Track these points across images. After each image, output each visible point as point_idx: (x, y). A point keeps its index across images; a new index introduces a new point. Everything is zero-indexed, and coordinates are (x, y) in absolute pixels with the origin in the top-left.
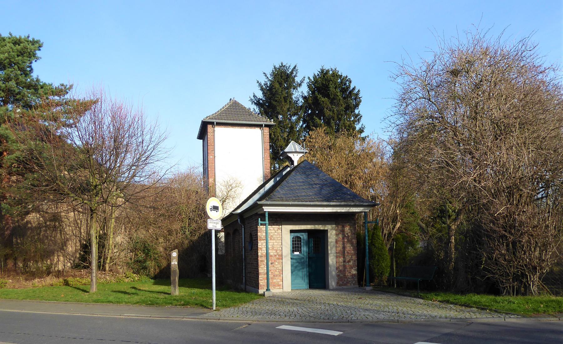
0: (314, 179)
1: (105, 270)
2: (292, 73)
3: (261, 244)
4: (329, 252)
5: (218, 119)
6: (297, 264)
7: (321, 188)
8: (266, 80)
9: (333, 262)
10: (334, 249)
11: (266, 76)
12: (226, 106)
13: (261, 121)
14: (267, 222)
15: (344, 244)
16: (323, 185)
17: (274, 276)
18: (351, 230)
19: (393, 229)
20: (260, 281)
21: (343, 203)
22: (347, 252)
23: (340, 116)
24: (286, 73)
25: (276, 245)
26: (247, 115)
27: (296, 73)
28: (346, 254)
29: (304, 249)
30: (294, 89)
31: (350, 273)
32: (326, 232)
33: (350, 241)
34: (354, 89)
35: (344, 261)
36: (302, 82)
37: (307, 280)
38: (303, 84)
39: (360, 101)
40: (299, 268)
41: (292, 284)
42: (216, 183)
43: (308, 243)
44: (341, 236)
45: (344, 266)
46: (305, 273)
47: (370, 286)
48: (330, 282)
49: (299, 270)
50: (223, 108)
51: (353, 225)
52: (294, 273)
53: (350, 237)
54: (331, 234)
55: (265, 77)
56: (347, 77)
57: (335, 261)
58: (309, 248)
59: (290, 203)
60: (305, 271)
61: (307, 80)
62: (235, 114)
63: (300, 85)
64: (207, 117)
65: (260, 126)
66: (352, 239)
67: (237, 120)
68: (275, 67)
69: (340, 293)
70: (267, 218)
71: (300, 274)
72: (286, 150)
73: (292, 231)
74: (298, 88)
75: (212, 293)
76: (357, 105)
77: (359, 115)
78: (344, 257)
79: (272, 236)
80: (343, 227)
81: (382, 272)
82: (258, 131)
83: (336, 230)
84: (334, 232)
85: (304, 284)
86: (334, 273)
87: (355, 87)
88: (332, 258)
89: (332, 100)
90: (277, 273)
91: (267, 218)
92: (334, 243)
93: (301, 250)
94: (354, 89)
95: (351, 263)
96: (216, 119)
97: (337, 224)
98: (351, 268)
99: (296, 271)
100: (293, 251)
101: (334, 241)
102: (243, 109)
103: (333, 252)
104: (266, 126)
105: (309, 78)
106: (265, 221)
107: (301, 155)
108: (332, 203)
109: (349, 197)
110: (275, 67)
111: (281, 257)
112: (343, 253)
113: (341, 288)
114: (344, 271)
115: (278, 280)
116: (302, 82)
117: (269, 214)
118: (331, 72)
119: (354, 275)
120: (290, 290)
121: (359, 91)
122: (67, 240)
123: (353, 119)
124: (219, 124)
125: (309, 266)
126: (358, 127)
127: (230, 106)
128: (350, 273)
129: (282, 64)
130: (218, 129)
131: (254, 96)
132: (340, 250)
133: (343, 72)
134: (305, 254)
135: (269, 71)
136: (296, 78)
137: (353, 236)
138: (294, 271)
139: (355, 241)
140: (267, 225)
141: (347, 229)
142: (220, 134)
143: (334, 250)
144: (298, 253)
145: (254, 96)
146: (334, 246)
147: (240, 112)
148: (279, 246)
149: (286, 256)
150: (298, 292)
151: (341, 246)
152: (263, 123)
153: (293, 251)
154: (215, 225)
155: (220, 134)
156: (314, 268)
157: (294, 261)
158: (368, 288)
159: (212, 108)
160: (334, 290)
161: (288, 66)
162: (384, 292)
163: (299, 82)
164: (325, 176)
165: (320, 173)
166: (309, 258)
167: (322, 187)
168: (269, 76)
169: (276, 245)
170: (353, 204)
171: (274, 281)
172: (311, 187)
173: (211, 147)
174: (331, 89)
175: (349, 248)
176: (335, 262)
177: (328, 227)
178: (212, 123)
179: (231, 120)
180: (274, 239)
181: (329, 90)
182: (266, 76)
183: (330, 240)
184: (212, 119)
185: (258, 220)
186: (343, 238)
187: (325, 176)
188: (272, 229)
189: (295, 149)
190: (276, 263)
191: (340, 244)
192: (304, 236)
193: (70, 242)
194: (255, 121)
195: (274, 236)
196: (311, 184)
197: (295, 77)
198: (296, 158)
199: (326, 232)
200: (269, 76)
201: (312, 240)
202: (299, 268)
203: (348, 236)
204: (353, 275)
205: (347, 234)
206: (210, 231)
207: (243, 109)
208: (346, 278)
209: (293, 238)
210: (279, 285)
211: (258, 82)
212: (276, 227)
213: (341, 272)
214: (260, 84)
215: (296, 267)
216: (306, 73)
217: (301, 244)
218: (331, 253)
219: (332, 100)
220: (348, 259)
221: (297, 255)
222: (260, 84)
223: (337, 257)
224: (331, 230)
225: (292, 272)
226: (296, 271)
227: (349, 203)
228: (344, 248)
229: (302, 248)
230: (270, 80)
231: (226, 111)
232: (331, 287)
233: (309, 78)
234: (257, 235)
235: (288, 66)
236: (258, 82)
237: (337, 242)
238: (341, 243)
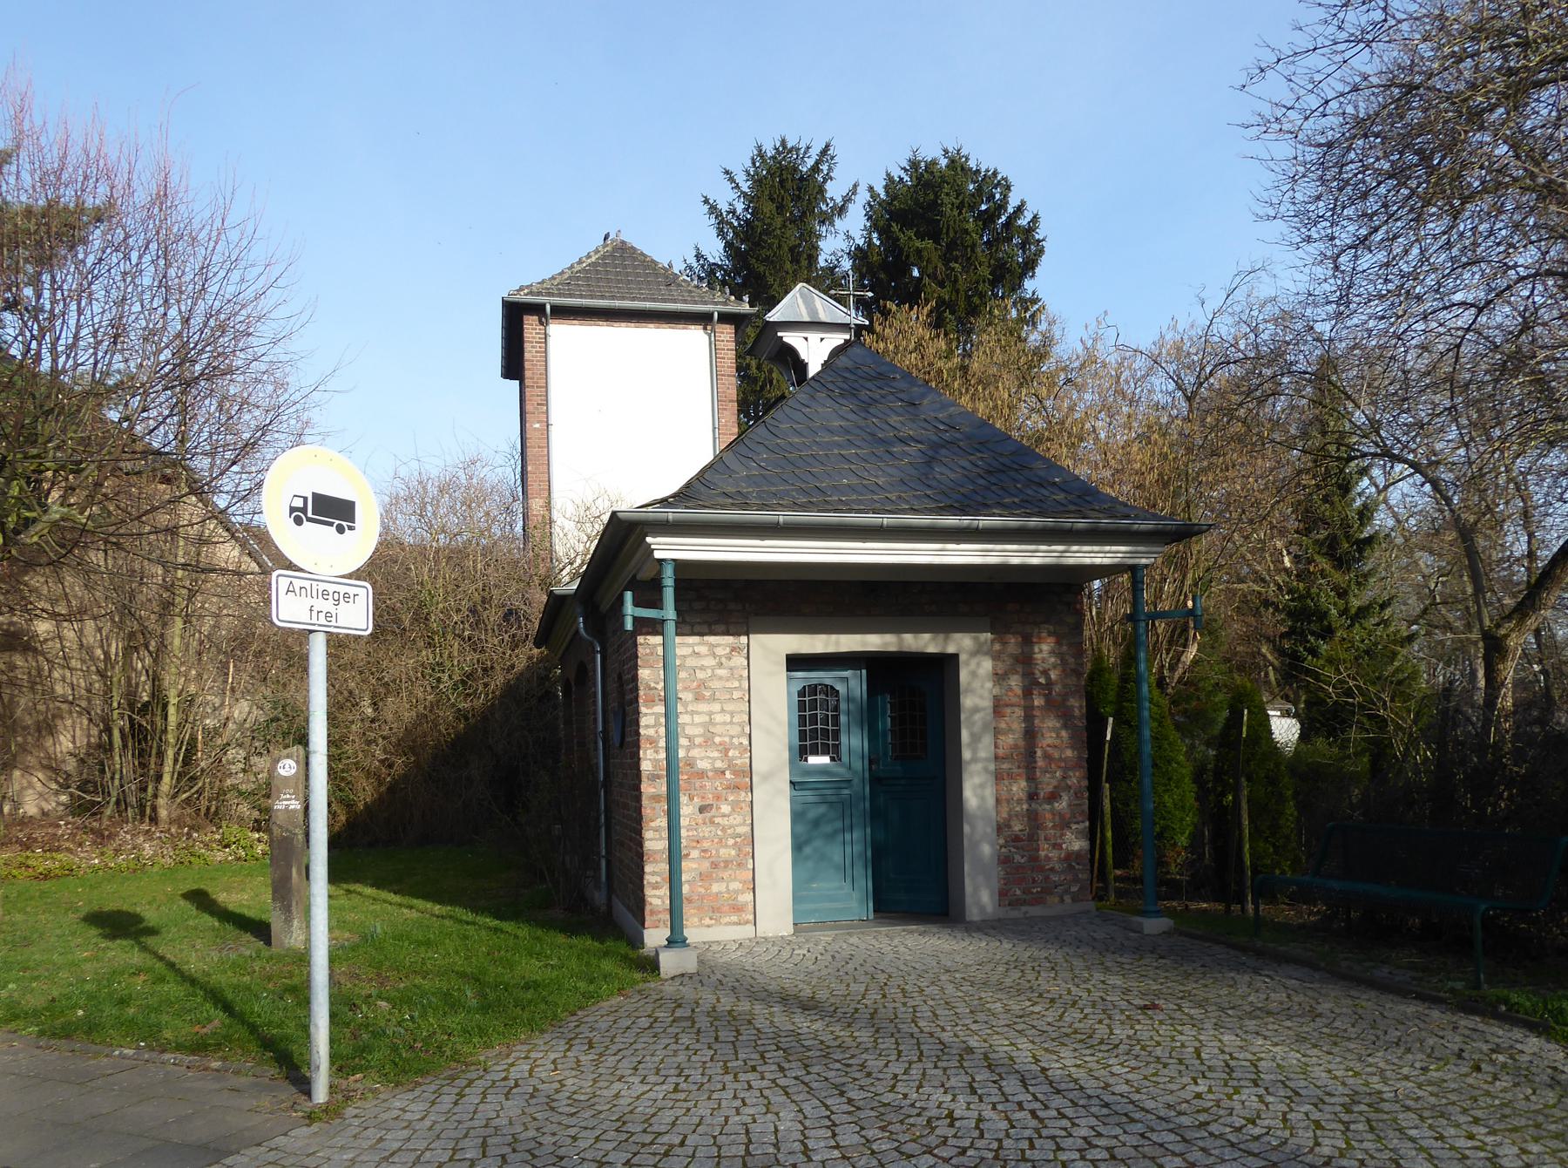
0: (894, 420)
1: (154, 820)
2: (815, 169)
3: (650, 720)
4: (966, 755)
5: (560, 295)
6: (822, 809)
7: (930, 461)
8: (733, 195)
9: (983, 799)
10: (987, 740)
11: (732, 180)
12: (589, 256)
13: (705, 303)
14: (669, 612)
15: (1028, 717)
16: (935, 447)
17: (715, 865)
18: (1061, 656)
19: (1172, 668)
20: (648, 892)
21: (1034, 522)
22: (1047, 756)
23: (976, 300)
24: (796, 169)
25: (725, 728)
26: (659, 283)
27: (830, 169)
28: (1040, 763)
29: (854, 741)
30: (822, 222)
31: (1057, 846)
32: (946, 664)
33: (1056, 706)
34: (1020, 210)
35: (1032, 796)
36: (847, 199)
37: (865, 883)
38: (851, 206)
39: (1041, 252)
40: (828, 829)
41: (797, 899)
42: (555, 515)
43: (869, 717)
44: (1015, 682)
45: (1033, 818)
46: (858, 848)
47: (1158, 913)
48: (968, 888)
49: (830, 837)
50: (580, 262)
51: (1070, 634)
52: (808, 850)
53: (1057, 688)
54: (974, 674)
55: (729, 185)
56: (995, 174)
57: (989, 794)
58: (873, 736)
59: (783, 517)
60: (857, 841)
61: (863, 197)
62: (619, 281)
63: (841, 210)
64: (521, 289)
65: (703, 319)
66: (1065, 696)
67: (623, 298)
68: (759, 148)
69: (1025, 951)
70: (669, 595)
71: (836, 853)
72: (775, 315)
73: (795, 662)
74: (837, 222)
75: (333, 981)
76: (1030, 266)
77: (1035, 301)
78: (1031, 778)
79: (703, 684)
80: (1027, 641)
81: (1164, 829)
82: (694, 339)
83: (996, 657)
84: (987, 665)
85: (849, 896)
86: (986, 850)
87: (1023, 203)
88: (977, 780)
89: (952, 244)
90: (728, 853)
91: (669, 595)
92: (988, 714)
93: (837, 748)
94: (1020, 210)
95: (1062, 805)
96: (549, 294)
97: (999, 628)
98: (1064, 824)
99: (818, 843)
100: (803, 752)
101: (987, 703)
102: (647, 267)
103: (982, 754)
104: (725, 318)
105: (871, 189)
106: (657, 603)
107: (838, 339)
108: (985, 522)
109: (1060, 497)
110: (759, 148)
111: (745, 778)
112: (1028, 756)
113: (1014, 914)
114: (1032, 837)
115: (735, 886)
116: (847, 199)
117: (676, 571)
118: (944, 162)
119: (1078, 854)
120: (786, 929)
121: (1035, 218)
122: (58, 715)
123: (1014, 313)
124: (563, 313)
125: (876, 816)
126: (1034, 338)
127: (604, 257)
128: (1057, 846)
129: (783, 143)
130: (560, 332)
131: (699, 256)
132: (1016, 746)
133: (982, 158)
134: (858, 765)
135: (741, 163)
136: (828, 185)
137: (1072, 681)
138: (807, 842)
139: (1077, 705)
140: (670, 627)
141: (1044, 650)
142: (567, 347)
143: (985, 749)
144: (824, 760)
145: (699, 256)
146: (985, 727)
147: (638, 275)
148: (735, 730)
149: (766, 778)
150: (825, 937)
151: (1018, 727)
152: (715, 309)
153: (803, 752)
154: (328, 606)
155: (567, 347)
156: (890, 812)
157: (809, 796)
158: (1154, 925)
159: (536, 265)
160: (990, 927)
161: (803, 145)
162: (1259, 954)
163: (839, 200)
164: (944, 406)
165: (923, 396)
166: (876, 781)
167: (934, 452)
168: (741, 178)
169: (725, 728)
170: (1081, 524)
171: (716, 888)
172: (880, 451)
173: (537, 391)
174: (947, 209)
175: (1054, 736)
176: (991, 802)
177: (960, 643)
178: (538, 310)
179: (603, 297)
180: (713, 699)
181: (941, 214)
182: (732, 180)
183: (967, 702)
184: (539, 294)
185: (620, 601)
186: (1027, 693)
187: (944, 406)
188: (703, 650)
189: (812, 310)
190: (725, 809)
191: (1014, 721)
192: (852, 684)
193: (69, 722)
194: (685, 302)
195: (715, 684)
196: (882, 441)
197: (825, 181)
198: (814, 351)
199: (946, 664)
200: (741, 178)
201: (886, 702)
202: (828, 829)
203: (1050, 683)
204: (1070, 857)
205: (1045, 673)
206: (292, 647)
207: (647, 267)
208: (1041, 869)
209: (802, 693)
210: (737, 909)
211: (706, 201)
212: (722, 642)
213: (1020, 847)
214: (713, 209)
215: (816, 823)
216: (861, 171)
217: (836, 719)
218: (974, 760)
219: (952, 244)
220: (1048, 783)
221: (821, 770)
222: (713, 209)
223: (998, 777)
224: (974, 654)
225: (798, 846)
226: (818, 843)
227: (1067, 522)
228: (1030, 734)
229: (844, 739)
230: (745, 194)
231: (587, 272)
232: (973, 914)
233: (871, 189)
234: (635, 678)
235: (803, 145)
236: (706, 201)
237: (998, 707)
238: (1019, 712)
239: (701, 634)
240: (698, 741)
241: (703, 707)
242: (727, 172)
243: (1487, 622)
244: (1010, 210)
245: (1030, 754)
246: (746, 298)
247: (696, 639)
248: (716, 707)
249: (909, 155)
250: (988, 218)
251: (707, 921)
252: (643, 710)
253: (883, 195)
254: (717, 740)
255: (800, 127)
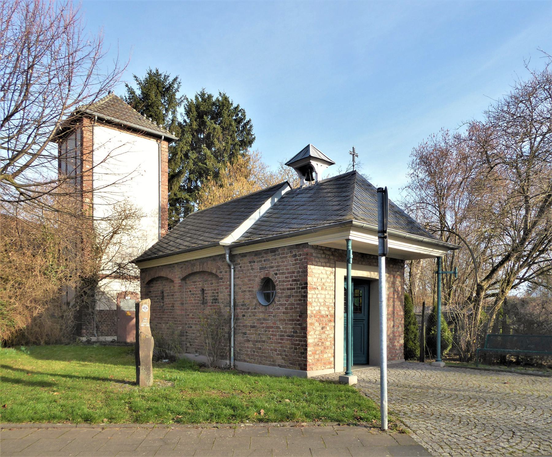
17: (325, 348)
65: (157, 137)
124: (101, 121)
135: (143, 76)
136: (177, 94)
178: (91, 117)
188: (324, 272)
197: (175, 92)
212: (329, 270)
216: (187, 92)
236: (127, 86)
239: (324, 266)
240: (322, 304)
241: (323, 292)
242: (135, 77)
243: (479, 281)
244: (245, 121)
245: (394, 313)
246: (174, 133)
247: (322, 268)
248: (326, 292)
249: (201, 90)
250: (239, 121)
251: (323, 368)
252: (309, 292)
253: (138, 92)
254: (327, 304)
255: (168, 71)
